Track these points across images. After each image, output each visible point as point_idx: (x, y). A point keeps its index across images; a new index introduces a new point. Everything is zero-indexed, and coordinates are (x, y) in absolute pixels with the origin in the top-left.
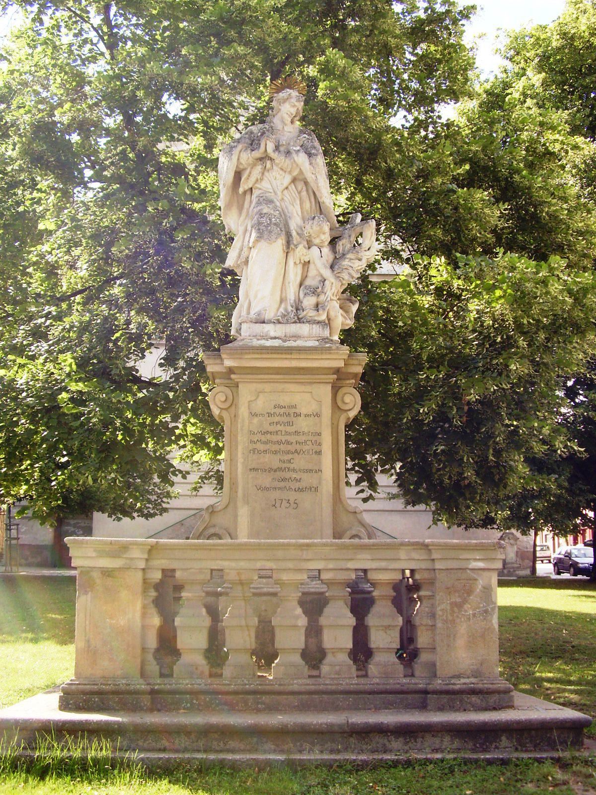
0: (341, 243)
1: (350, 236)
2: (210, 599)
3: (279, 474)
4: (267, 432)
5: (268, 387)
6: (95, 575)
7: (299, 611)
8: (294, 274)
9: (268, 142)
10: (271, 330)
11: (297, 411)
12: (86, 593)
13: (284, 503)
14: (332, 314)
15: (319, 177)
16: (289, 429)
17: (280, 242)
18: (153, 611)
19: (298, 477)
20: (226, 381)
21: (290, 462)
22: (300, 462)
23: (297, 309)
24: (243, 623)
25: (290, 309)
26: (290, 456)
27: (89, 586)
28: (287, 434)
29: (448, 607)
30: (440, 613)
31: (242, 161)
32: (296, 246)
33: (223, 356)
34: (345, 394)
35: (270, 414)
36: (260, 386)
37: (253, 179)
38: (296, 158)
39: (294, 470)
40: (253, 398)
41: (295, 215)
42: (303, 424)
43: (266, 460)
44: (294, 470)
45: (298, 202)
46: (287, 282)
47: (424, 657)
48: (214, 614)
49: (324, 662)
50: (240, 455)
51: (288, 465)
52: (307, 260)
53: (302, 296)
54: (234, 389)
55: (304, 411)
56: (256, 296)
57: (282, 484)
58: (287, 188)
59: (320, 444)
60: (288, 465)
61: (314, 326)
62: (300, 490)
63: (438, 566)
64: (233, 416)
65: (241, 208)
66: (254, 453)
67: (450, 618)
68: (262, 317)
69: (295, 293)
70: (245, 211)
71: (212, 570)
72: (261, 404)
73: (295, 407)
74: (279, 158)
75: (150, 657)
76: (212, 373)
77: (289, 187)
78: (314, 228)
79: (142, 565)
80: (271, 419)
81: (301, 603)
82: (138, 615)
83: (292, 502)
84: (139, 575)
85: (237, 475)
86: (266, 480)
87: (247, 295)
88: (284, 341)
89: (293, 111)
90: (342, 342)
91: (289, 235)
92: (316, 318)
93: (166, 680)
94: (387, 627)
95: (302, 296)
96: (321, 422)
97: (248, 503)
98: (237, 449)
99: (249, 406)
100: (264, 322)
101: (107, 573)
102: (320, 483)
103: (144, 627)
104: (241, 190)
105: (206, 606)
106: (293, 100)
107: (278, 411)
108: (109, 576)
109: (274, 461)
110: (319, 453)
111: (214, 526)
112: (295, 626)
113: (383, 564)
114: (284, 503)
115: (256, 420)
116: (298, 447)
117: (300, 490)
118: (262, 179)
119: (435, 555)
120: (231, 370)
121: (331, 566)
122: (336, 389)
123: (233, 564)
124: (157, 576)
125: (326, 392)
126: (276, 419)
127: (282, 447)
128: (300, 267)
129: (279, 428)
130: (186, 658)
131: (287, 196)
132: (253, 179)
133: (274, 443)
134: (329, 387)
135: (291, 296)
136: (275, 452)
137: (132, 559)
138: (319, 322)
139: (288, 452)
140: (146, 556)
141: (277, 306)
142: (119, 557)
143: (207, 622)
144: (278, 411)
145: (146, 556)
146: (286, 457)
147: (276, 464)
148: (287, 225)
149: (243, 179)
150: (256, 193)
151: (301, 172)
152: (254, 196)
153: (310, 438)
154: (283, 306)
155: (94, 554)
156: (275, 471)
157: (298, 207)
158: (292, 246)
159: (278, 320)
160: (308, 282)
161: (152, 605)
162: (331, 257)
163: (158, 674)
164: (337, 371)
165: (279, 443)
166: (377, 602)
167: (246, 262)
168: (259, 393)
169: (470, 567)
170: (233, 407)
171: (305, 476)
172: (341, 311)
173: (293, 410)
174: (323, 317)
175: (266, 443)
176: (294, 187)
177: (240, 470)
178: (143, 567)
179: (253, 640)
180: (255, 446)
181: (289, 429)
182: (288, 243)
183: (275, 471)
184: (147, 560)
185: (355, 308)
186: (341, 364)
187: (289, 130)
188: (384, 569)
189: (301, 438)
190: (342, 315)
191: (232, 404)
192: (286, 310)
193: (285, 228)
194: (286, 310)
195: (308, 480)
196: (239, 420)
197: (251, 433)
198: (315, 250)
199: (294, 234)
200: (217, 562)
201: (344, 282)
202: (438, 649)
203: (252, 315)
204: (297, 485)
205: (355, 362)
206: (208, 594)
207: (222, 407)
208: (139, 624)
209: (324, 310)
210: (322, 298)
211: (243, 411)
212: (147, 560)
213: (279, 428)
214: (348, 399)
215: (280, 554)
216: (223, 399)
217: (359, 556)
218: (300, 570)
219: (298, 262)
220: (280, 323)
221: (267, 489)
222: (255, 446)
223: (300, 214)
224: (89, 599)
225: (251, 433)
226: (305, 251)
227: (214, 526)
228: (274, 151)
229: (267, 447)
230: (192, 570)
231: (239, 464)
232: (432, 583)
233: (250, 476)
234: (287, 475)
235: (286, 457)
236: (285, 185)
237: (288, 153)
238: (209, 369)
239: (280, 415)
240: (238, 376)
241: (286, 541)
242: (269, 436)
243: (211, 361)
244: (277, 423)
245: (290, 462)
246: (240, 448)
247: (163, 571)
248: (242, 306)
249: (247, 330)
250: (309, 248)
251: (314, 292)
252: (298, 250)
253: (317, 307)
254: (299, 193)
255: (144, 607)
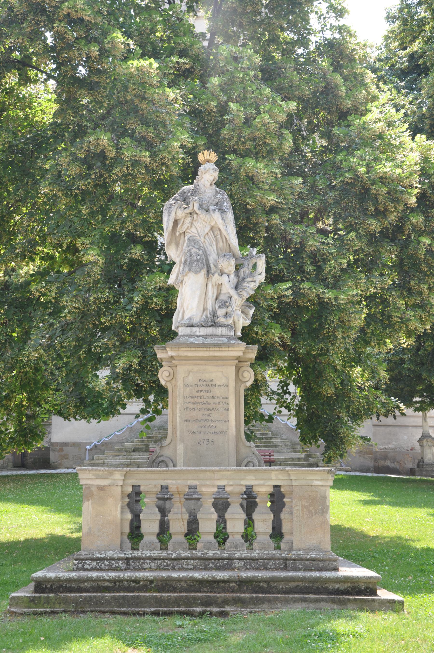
0: (242, 270)
1: (248, 265)
2: (161, 502)
3: (203, 423)
4: (195, 397)
5: (195, 368)
6: (94, 489)
7: (213, 509)
8: (212, 292)
9: (195, 203)
10: (198, 331)
11: (214, 383)
12: (88, 500)
13: (206, 442)
14: (236, 319)
15: (228, 227)
16: (209, 395)
17: (203, 272)
18: (127, 510)
19: (214, 425)
20: (169, 364)
21: (209, 415)
22: (215, 416)
23: (214, 316)
24: (180, 517)
25: (209, 316)
26: (209, 412)
27: (90, 496)
28: (207, 397)
29: (300, 508)
30: (295, 512)
31: (178, 214)
32: (213, 274)
33: (168, 349)
34: (244, 371)
35: (197, 385)
36: (190, 368)
37: (185, 226)
38: (213, 215)
39: (212, 421)
40: (186, 375)
41: (213, 252)
42: (217, 392)
43: (194, 414)
44: (212, 421)
45: (214, 243)
46: (207, 298)
47: (287, 537)
48: (163, 512)
49: (227, 541)
50: (178, 411)
51: (208, 418)
52: (220, 283)
53: (217, 307)
54: (174, 368)
55: (218, 383)
56: (188, 307)
57: (204, 430)
58: (207, 234)
59: (228, 404)
60: (208, 418)
61: (224, 328)
62: (216, 433)
63: (294, 483)
64: (173, 385)
65: (177, 245)
66: (187, 410)
67: (301, 515)
68: (191, 322)
69: (212, 305)
70: (180, 247)
71: (162, 486)
72: (191, 379)
73: (212, 380)
74: (202, 215)
75: (125, 537)
76: (161, 359)
77: (209, 234)
78: (225, 262)
79: (121, 483)
80: (197, 389)
81: (215, 505)
82: (119, 512)
83: (210, 441)
84: (119, 489)
85: (176, 423)
86: (194, 427)
87: (182, 304)
88: (206, 338)
89: (212, 178)
90: (241, 339)
91: (208, 267)
92: (225, 323)
93: (135, 552)
94: (265, 520)
95: (217, 307)
96: (228, 390)
97: (183, 442)
98: (176, 407)
99: (184, 380)
100: (192, 326)
101: (101, 488)
102: (228, 429)
103: (122, 520)
104: (178, 234)
105: (158, 507)
106: (212, 171)
107: (201, 383)
108: (102, 490)
109: (199, 415)
110: (227, 410)
111: (162, 456)
112: (210, 519)
113: (262, 482)
114: (206, 442)
115: (188, 389)
116: (214, 406)
117: (216, 433)
118: (191, 227)
119: (292, 478)
120: (172, 357)
121: (231, 483)
122: (238, 369)
123: (174, 482)
124: (130, 489)
125: (232, 370)
126: (201, 388)
127: (204, 406)
128: (216, 288)
129: (202, 394)
130: (146, 538)
131: (208, 239)
132: (185, 226)
133: (199, 403)
134: (234, 367)
135: (210, 308)
136: (200, 410)
137: (115, 479)
138: (227, 326)
139: (208, 410)
140: (123, 478)
141: (201, 314)
142: (108, 478)
143: (158, 516)
144: (201, 383)
145: (123, 478)
146: (207, 413)
147: (200, 417)
148: (207, 260)
149: (179, 226)
150: (188, 236)
151: (216, 223)
152: (186, 238)
153: (222, 400)
154: (205, 313)
155: (93, 477)
156: (200, 421)
157: (215, 247)
158: (211, 275)
159: (202, 324)
160: (222, 297)
161: (127, 507)
162: (235, 280)
163: (130, 548)
164: (238, 359)
165: (202, 403)
166: (232, 504)
167: (182, 282)
168: (189, 372)
169: (313, 484)
170: (174, 379)
171: (218, 424)
172: (242, 315)
173: (211, 383)
174: (230, 321)
175: (194, 403)
176: (212, 233)
177: (178, 420)
178: (122, 484)
179: (186, 527)
180: (187, 405)
181: (209, 395)
182: (208, 272)
183: (200, 421)
184: (124, 480)
185: (252, 312)
186: (241, 354)
187: (209, 192)
188: (262, 485)
189: (217, 400)
190: (243, 318)
191: (173, 377)
192: (207, 317)
193: (206, 262)
194: (207, 317)
195: (220, 427)
196: (178, 389)
197: (185, 397)
198: (225, 277)
199: (212, 266)
200: (166, 481)
201: (244, 298)
202: (294, 533)
203: (185, 322)
204: (214, 430)
205: (250, 351)
206: (159, 499)
207: (167, 380)
208: (120, 518)
209: (230, 317)
210: (230, 309)
211: (180, 383)
212: (124, 480)
213: (202, 394)
214: (246, 374)
215: (201, 475)
216: (168, 375)
217: (247, 477)
218: (213, 486)
219: (214, 285)
220: (203, 326)
221: (195, 432)
222: (187, 405)
223: (216, 251)
224: (90, 504)
225: (185, 397)
226: (219, 277)
227: (162, 456)
228: (199, 209)
229: (195, 406)
230: (150, 486)
231: (178, 417)
232: (291, 493)
233: (184, 425)
234: (208, 424)
235: (207, 413)
236: (206, 232)
237: (207, 210)
238: (159, 356)
239: (203, 386)
240: (177, 362)
241: (204, 468)
242: (196, 399)
243: (160, 351)
244: (201, 391)
245: (209, 415)
246: (178, 407)
247: (133, 486)
248: (179, 312)
249: (181, 331)
250: (222, 275)
251: (224, 305)
252: (214, 277)
253: (226, 315)
254: (215, 237)
255: (122, 508)
